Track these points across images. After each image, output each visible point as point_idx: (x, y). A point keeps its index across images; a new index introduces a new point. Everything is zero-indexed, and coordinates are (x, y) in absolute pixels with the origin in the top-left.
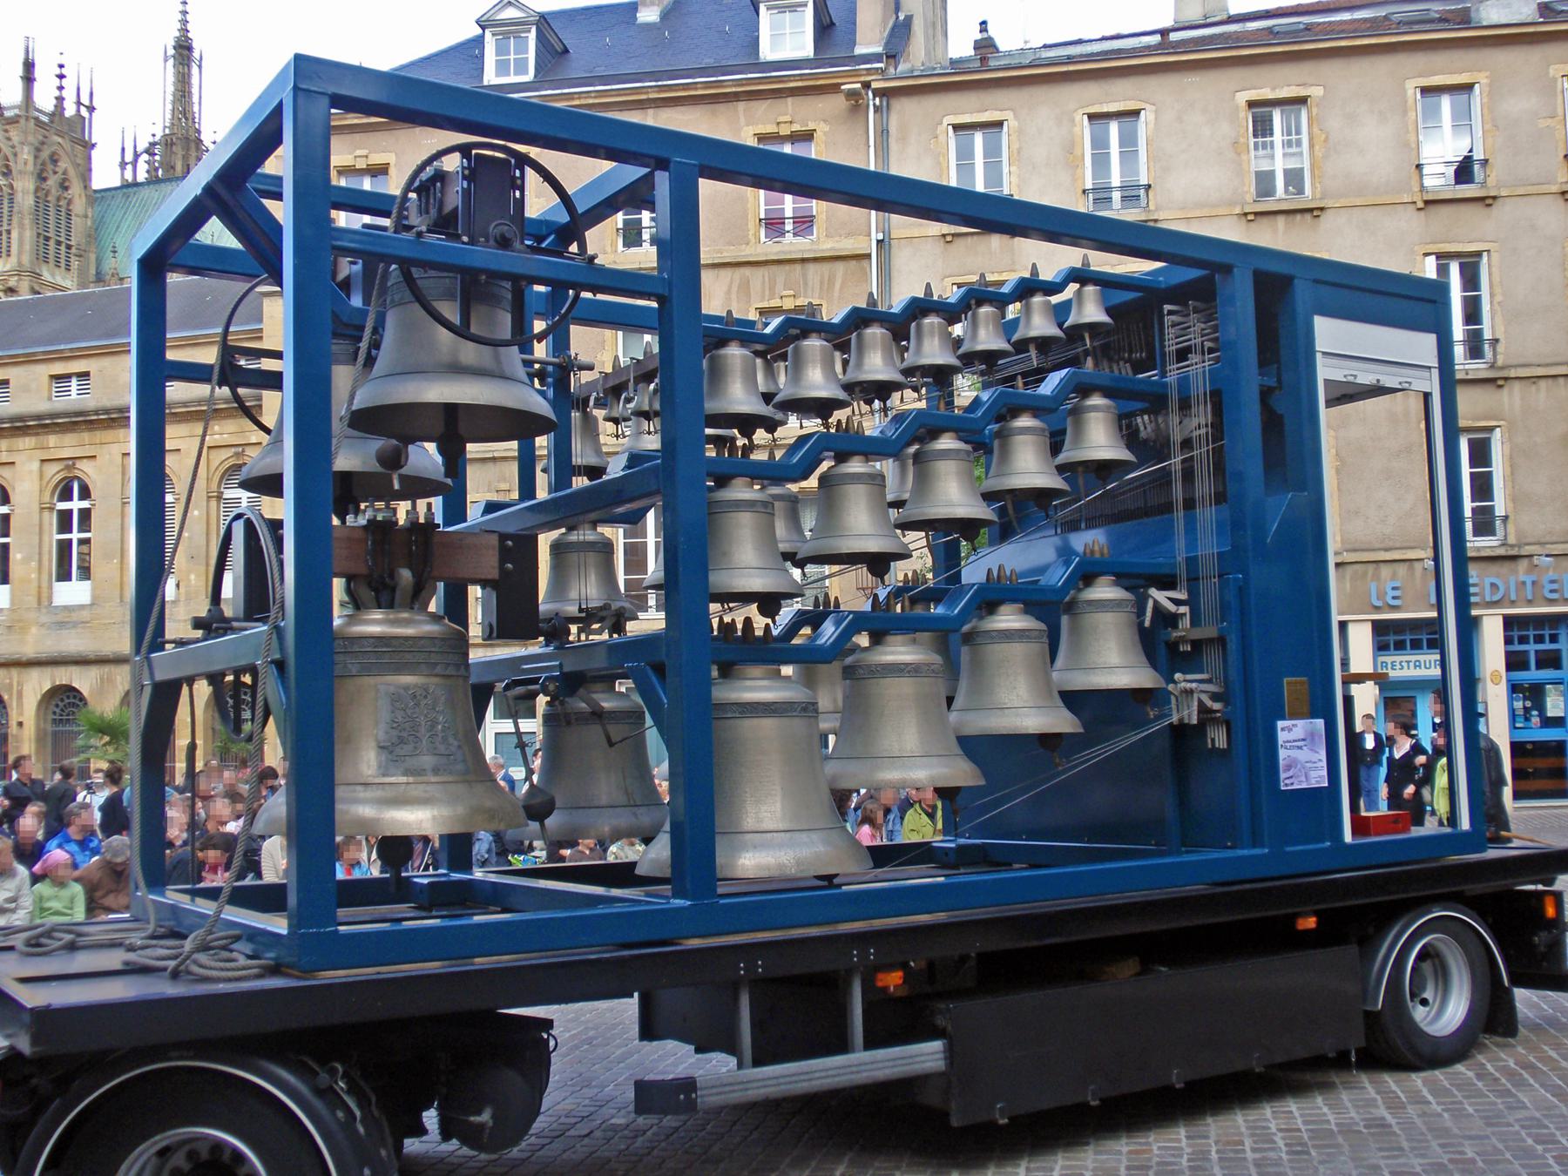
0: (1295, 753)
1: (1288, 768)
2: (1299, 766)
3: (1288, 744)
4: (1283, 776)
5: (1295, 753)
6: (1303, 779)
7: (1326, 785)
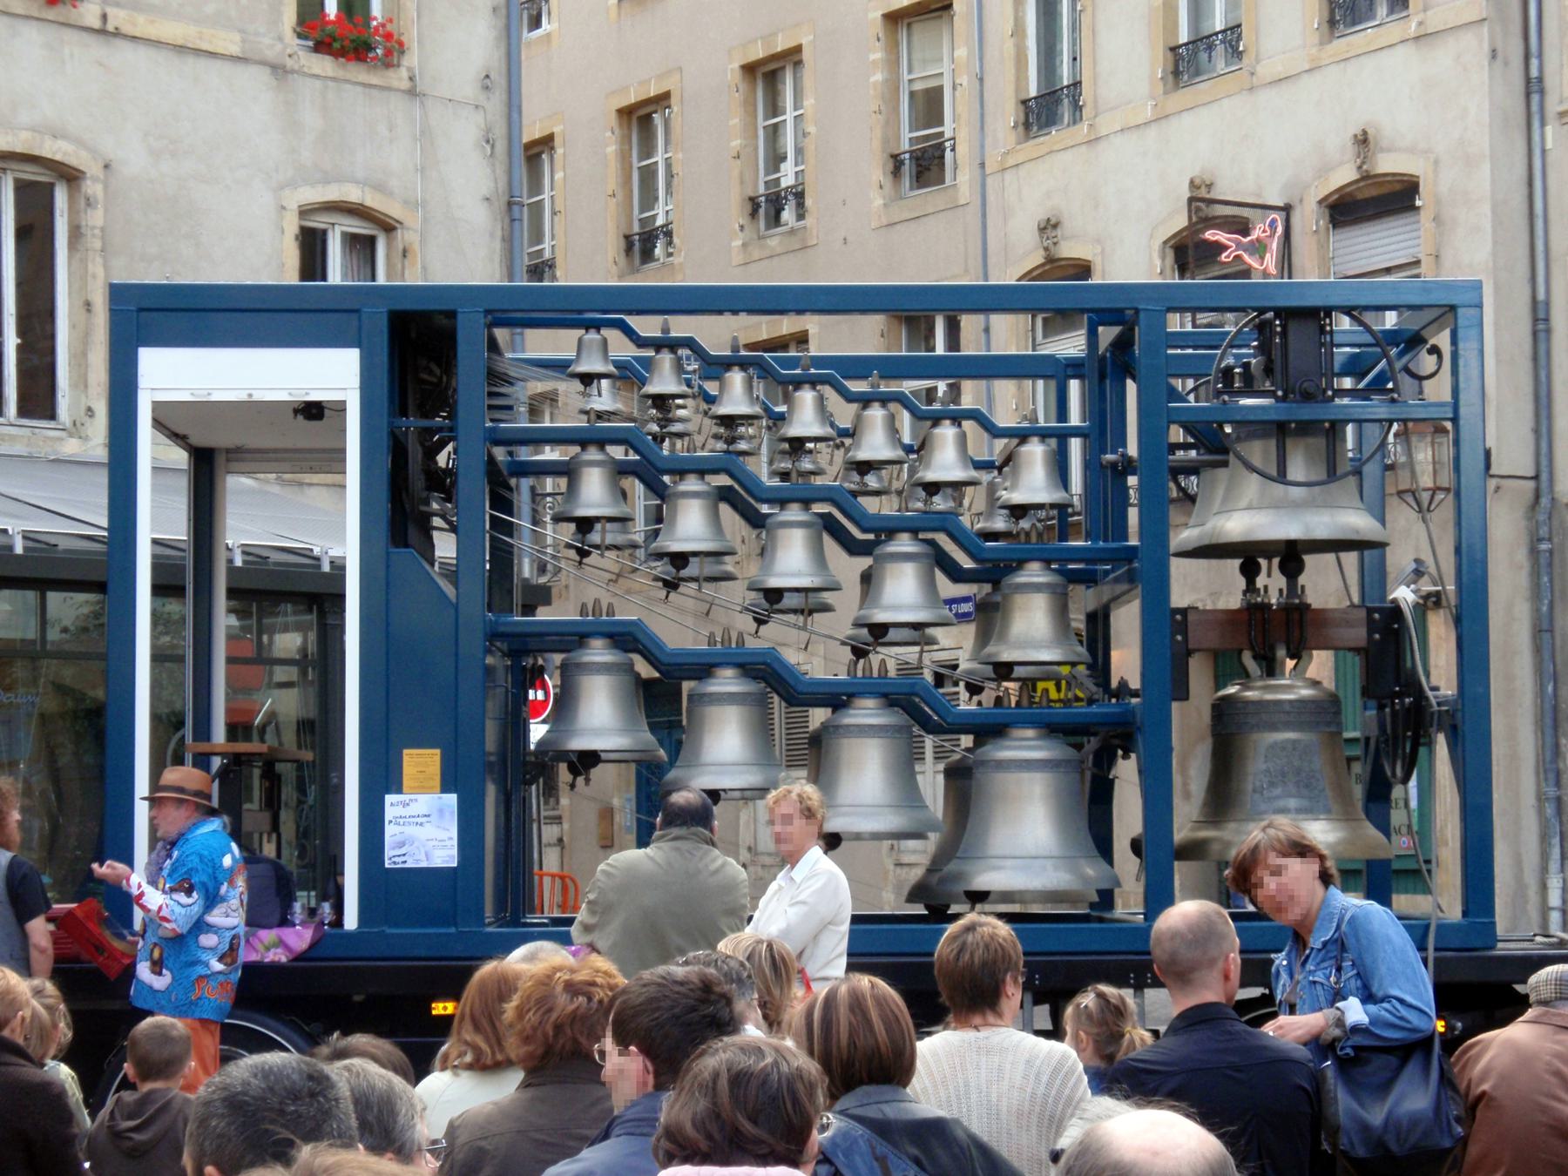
0: (411, 830)
1: (402, 844)
2: (416, 844)
3: (402, 821)
4: (388, 853)
5: (411, 830)
6: (424, 858)
7: (406, 752)
